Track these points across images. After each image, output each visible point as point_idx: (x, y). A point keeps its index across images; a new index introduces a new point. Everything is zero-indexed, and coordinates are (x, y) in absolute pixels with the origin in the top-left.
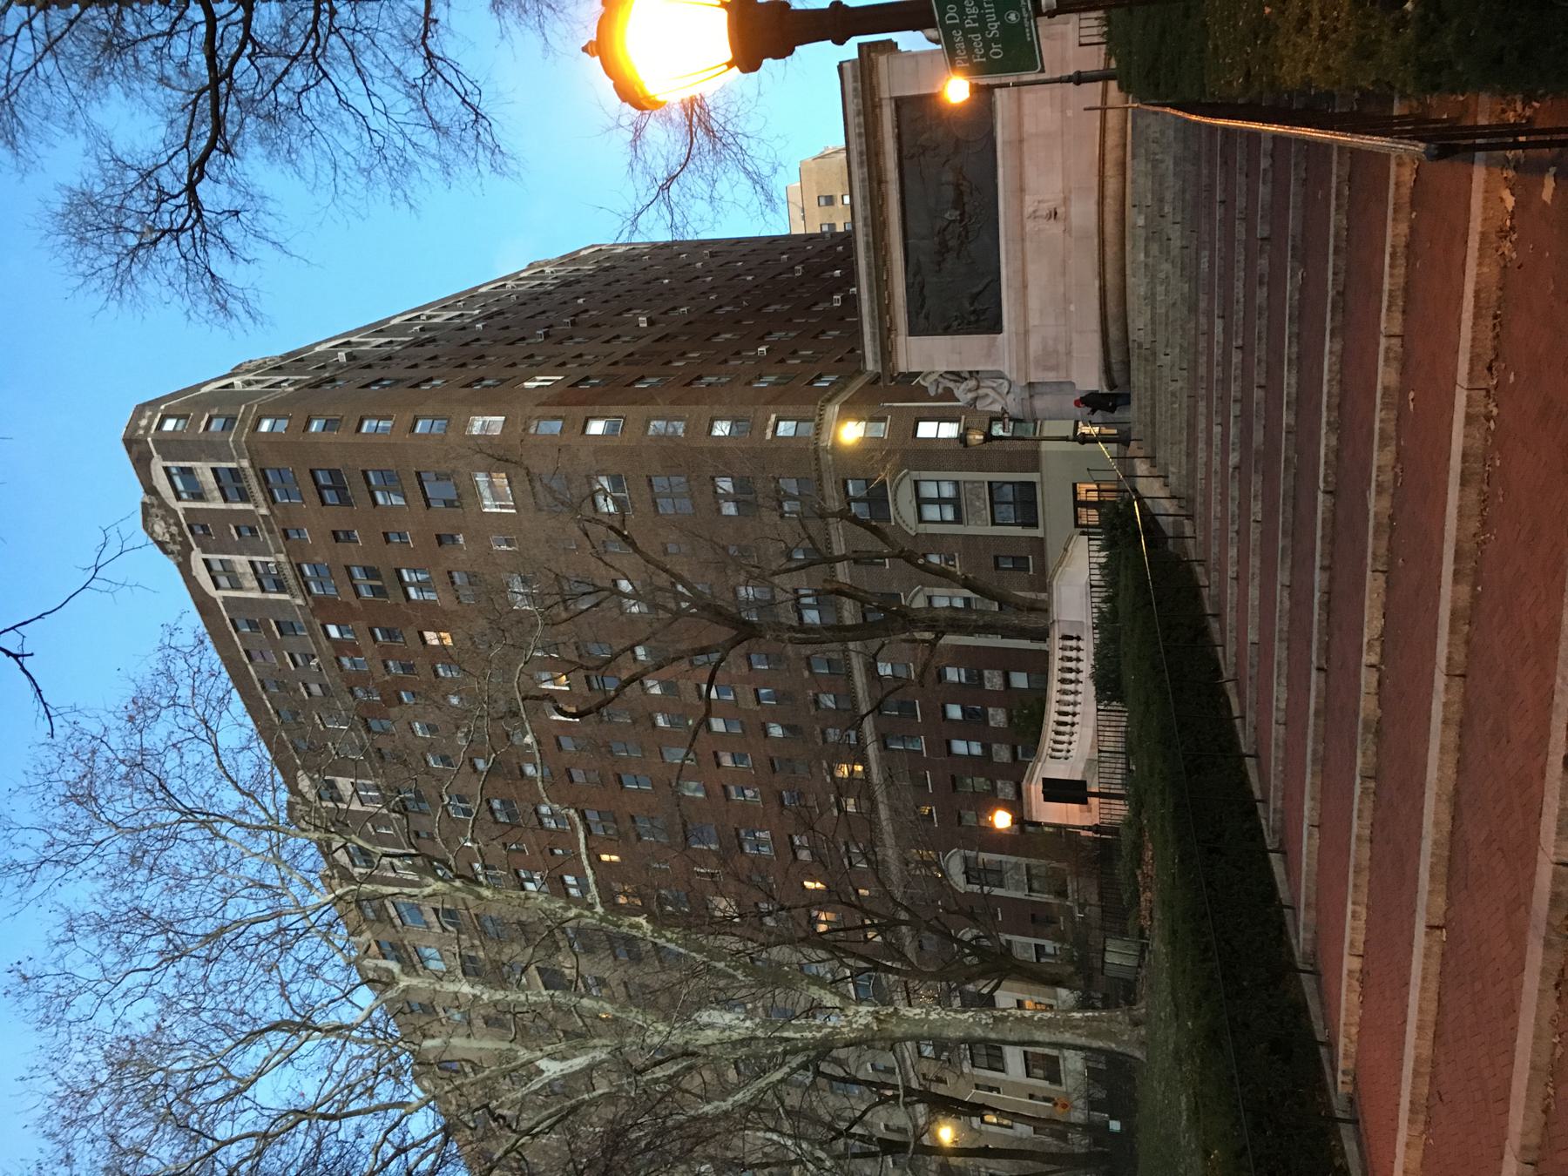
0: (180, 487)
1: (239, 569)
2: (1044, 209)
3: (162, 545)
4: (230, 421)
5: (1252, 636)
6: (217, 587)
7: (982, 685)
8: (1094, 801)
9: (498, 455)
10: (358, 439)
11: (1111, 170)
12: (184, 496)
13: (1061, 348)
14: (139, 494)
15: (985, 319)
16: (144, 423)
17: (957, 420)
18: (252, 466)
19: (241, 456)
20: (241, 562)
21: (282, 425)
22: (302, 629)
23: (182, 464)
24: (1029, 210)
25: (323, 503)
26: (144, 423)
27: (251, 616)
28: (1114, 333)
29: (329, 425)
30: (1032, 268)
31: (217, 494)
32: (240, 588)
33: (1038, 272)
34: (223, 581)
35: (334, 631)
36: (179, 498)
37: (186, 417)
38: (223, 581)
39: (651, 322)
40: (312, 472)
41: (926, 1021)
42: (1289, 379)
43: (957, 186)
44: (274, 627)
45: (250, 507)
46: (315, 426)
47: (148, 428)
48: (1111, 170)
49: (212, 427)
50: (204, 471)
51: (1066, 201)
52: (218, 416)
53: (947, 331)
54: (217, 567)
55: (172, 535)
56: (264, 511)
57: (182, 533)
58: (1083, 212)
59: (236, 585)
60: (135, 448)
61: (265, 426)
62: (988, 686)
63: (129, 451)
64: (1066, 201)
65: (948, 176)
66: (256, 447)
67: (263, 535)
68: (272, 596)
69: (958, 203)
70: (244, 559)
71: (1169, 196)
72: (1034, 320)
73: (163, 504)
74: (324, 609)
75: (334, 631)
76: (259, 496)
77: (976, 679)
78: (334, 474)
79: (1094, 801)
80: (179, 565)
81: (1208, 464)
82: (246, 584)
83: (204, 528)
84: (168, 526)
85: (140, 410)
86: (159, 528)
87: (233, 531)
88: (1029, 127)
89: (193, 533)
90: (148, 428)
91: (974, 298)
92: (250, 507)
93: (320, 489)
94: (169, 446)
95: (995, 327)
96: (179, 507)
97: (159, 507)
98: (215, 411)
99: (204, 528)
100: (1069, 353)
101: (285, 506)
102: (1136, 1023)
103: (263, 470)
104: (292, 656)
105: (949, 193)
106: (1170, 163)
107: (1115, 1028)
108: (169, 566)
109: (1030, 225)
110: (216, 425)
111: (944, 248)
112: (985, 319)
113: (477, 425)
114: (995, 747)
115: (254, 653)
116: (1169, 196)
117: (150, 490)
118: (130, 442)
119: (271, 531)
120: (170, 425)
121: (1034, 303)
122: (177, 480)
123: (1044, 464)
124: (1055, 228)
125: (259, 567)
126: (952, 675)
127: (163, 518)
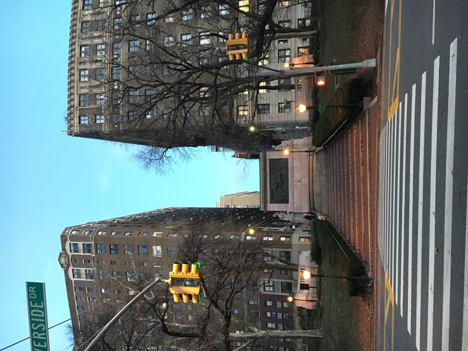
0: (72, 248)
1: (82, 272)
2: (297, 180)
3: (62, 265)
4: (91, 232)
5: (339, 213)
6: (74, 277)
7: (276, 306)
8: (310, 289)
9: (159, 241)
10: (124, 237)
11: (310, 171)
12: (72, 251)
13: (301, 207)
14: (60, 250)
15: (286, 201)
16: (67, 232)
17: (273, 237)
18: (94, 243)
19: (92, 240)
20: (83, 270)
21: (104, 233)
22: (94, 290)
23: (75, 242)
24: (294, 180)
25: (111, 254)
26: (67, 232)
27: (81, 287)
28: (312, 206)
29: (118, 233)
30: (295, 191)
31: (82, 251)
32: (80, 278)
33: (296, 192)
34: (76, 276)
35: (103, 291)
36: (71, 252)
37: (79, 231)
38: (76, 276)
39: (193, 219)
40: (110, 245)
41: (277, 332)
42: (342, 169)
43: (281, 175)
44: (87, 290)
45: (91, 254)
46: (113, 234)
47: (68, 233)
48: (310, 171)
49: (85, 233)
50: (80, 244)
51: (302, 179)
52: (87, 231)
53: (278, 203)
54: (75, 271)
55: (66, 262)
56: (94, 255)
57: (69, 262)
58: (305, 181)
59: (79, 276)
60: (63, 238)
61: (100, 233)
62: (278, 307)
63: (61, 239)
64: (302, 179)
65: (279, 174)
66: (97, 239)
67: (92, 262)
68: (88, 280)
69: (281, 178)
70: (84, 269)
71: (323, 166)
72: (295, 201)
73: (66, 253)
74: (102, 284)
75: (103, 291)
76: (94, 251)
77: (275, 305)
78: (116, 246)
79: (310, 289)
80: (65, 271)
81: (331, 206)
82: (82, 276)
83: (76, 260)
84: (65, 259)
85: (66, 229)
86: (63, 260)
87: (83, 261)
88: (295, 165)
89: (72, 261)
90: (68, 233)
91: (284, 196)
92: (91, 254)
93: (111, 249)
94: (72, 238)
95: (288, 202)
96: (70, 254)
97: (65, 254)
98: (87, 230)
99: (76, 260)
100: (302, 208)
101: (100, 254)
102: (321, 331)
103: (97, 244)
104: (89, 298)
105: (279, 177)
106: (323, 161)
107: (316, 332)
108: (62, 271)
109: (295, 183)
110: (87, 233)
111: (278, 187)
112: (286, 201)
113: (155, 235)
114: (279, 325)
115: (78, 298)
116: (323, 166)
117: (64, 249)
118: (62, 236)
119: (94, 261)
120: (74, 233)
121: (295, 197)
122: (72, 247)
123: (292, 248)
124: (300, 184)
125: (87, 272)
126: (269, 303)
127: (65, 258)
